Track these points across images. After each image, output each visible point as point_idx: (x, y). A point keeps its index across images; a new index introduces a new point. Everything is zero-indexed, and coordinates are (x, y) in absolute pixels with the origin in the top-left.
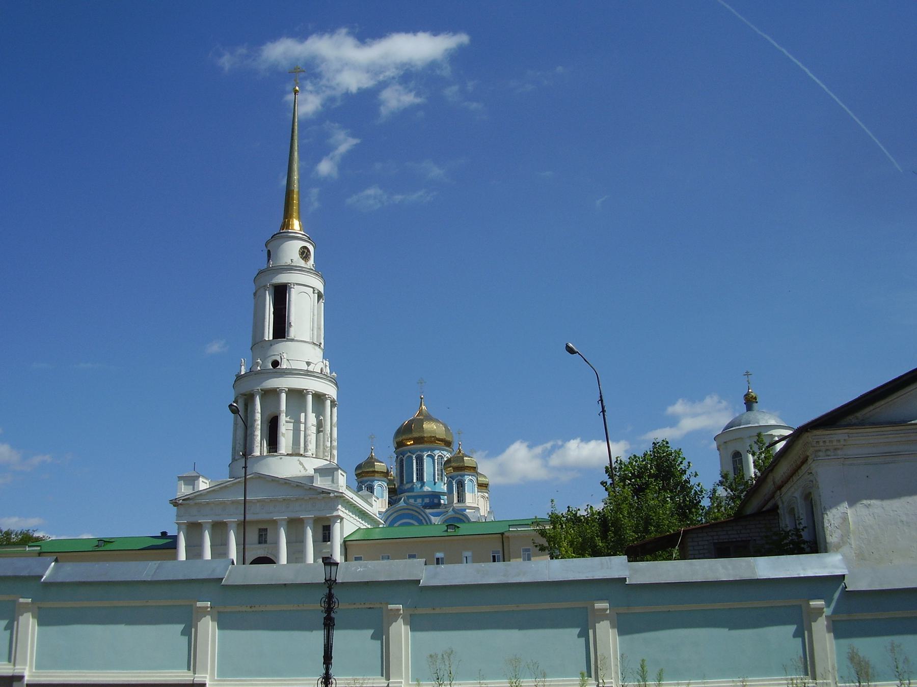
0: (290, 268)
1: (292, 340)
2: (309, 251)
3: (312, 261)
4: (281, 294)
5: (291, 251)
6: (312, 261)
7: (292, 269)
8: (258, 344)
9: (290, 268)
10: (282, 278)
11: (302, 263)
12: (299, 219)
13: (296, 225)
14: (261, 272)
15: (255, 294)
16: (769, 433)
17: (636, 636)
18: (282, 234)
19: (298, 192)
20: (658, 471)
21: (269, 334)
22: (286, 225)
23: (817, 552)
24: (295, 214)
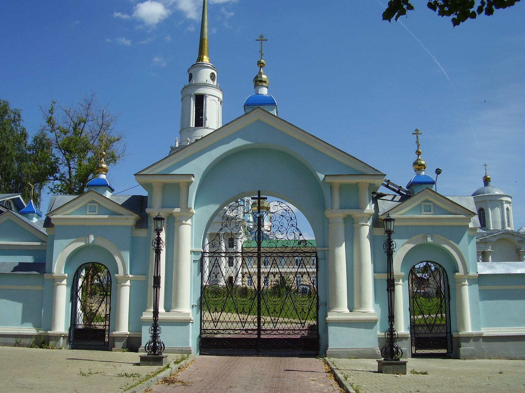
0: (206, 85)
1: (207, 128)
2: (215, 76)
3: (215, 82)
4: (200, 100)
5: (205, 75)
6: (215, 82)
7: (207, 86)
8: (184, 129)
9: (206, 85)
10: (201, 91)
11: (211, 82)
12: (208, 56)
13: (206, 59)
14: (185, 87)
15: (182, 99)
16: (501, 199)
17: (515, 342)
18: (199, 64)
19: (208, 39)
20: (173, 149)
21: (192, 124)
22: (200, 59)
23: (379, 227)
24: (206, 53)
